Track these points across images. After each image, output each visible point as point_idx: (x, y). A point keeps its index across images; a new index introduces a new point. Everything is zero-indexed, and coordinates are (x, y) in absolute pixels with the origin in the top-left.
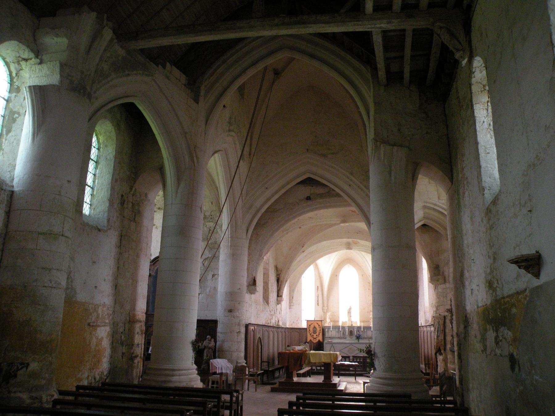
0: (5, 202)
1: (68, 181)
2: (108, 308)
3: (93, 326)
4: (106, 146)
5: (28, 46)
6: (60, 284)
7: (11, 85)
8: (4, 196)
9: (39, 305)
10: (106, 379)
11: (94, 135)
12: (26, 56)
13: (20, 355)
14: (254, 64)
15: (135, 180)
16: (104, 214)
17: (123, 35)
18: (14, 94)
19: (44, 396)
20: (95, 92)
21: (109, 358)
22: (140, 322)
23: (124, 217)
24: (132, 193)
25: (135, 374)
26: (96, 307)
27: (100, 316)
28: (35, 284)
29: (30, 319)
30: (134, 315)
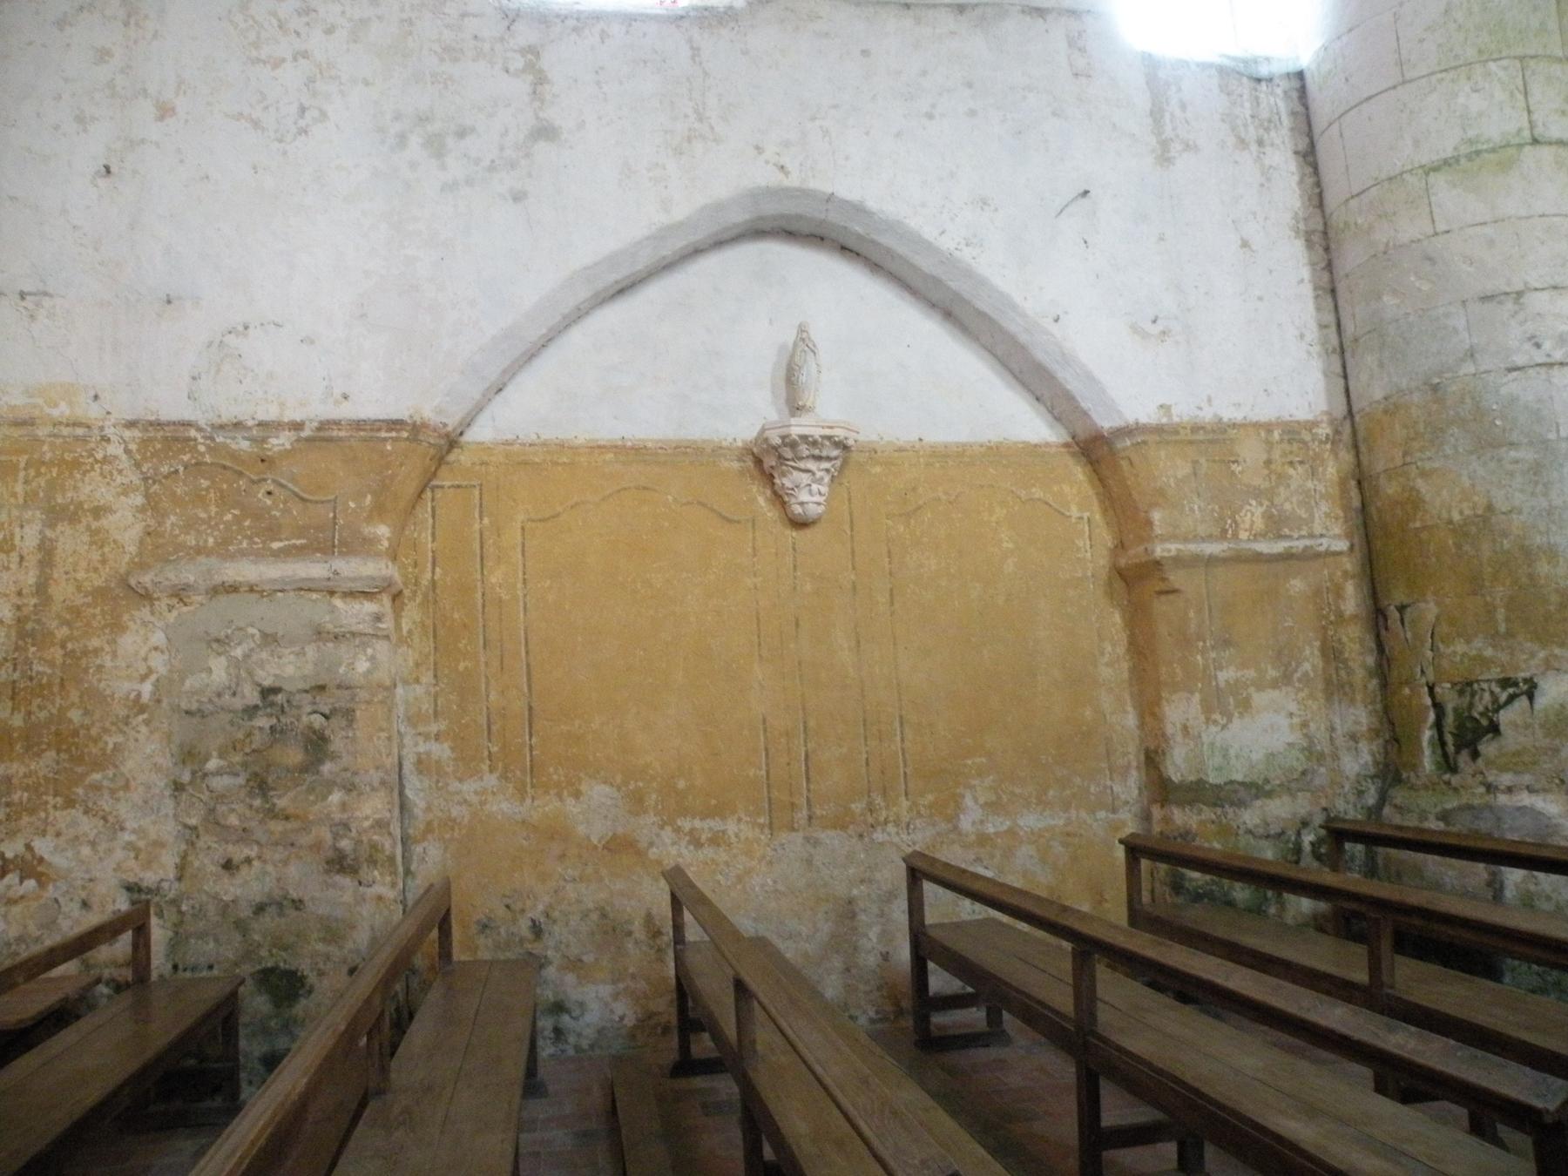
0: (1286, 121)
8: (1278, 102)
13: (1489, 652)
28: (1469, 368)
29: (1490, 508)
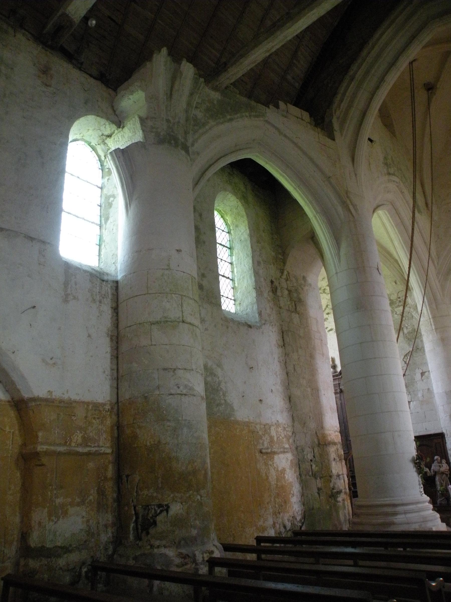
0: (110, 296)
1: (177, 250)
2: (285, 428)
3: (267, 453)
4: (237, 226)
5: (108, 119)
6: (191, 389)
7: (102, 170)
8: (108, 289)
9: (169, 421)
10: (301, 527)
11: (216, 213)
12: (108, 132)
13: (155, 494)
14: (392, 64)
15: (284, 262)
16: (253, 307)
17: (209, 73)
18: (106, 179)
19: (197, 553)
20: (193, 145)
21: (299, 497)
22: (335, 444)
23: (280, 308)
24: (284, 277)
25: (342, 518)
26: (267, 428)
27: (275, 439)
28: (157, 392)
29: (159, 442)
30: (324, 436)
